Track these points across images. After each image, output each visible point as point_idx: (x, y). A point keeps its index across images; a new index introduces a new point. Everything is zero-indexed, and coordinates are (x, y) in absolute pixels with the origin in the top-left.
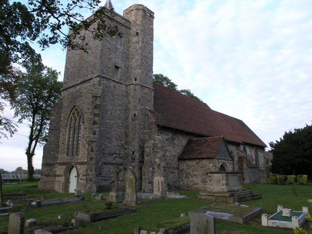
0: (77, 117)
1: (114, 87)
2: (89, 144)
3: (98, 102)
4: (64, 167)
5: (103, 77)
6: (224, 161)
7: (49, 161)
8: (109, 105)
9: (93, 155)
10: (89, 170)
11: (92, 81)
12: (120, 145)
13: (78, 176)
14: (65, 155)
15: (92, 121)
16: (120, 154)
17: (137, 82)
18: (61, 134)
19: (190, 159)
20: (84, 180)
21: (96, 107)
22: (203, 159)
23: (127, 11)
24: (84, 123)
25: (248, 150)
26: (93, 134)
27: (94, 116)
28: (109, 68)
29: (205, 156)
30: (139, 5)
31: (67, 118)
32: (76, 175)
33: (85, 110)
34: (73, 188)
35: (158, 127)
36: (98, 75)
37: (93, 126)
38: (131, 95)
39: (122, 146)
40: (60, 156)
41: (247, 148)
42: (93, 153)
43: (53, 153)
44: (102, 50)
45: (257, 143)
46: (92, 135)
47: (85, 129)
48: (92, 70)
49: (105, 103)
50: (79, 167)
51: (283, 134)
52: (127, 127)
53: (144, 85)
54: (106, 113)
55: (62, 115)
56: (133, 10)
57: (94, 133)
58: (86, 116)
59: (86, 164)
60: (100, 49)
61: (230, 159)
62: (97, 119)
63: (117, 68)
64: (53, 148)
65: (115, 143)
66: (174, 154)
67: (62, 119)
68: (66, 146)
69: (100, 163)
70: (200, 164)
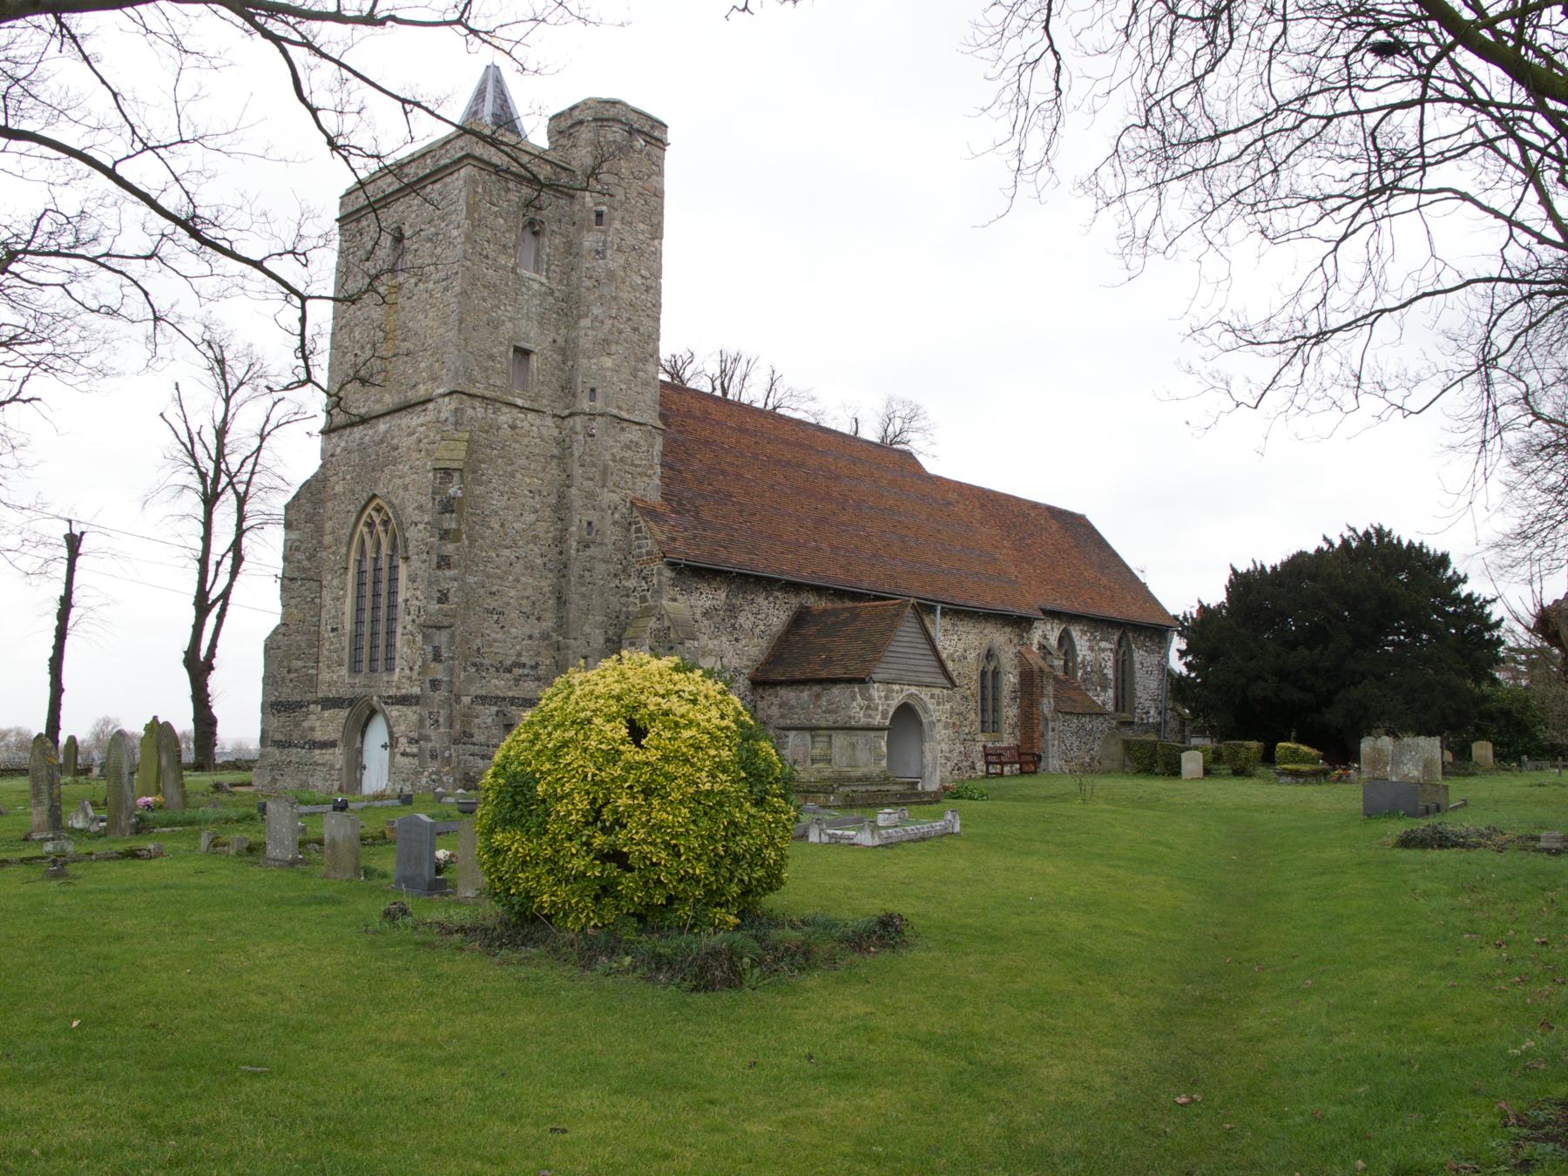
0: (382, 536)
1: (513, 427)
2: (425, 636)
3: (454, 490)
4: (345, 713)
5: (470, 395)
6: (913, 689)
7: (287, 693)
9: (439, 672)
10: (428, 722)
11: (431, 406)
12: (536, 633)
13: (392, 744)
14: (344, 671)
15: (435, 559)
16: (535, 667)
17: (599, 405)
18: (327, 596)
19: (792, 683)
20: (414, 756)
21: (448, 506)
22: (835, 681)
23: (564, 124)
24: (407, 559)
25: (1082, 642)
26: (440, 601)
27: (441, 538)
28: (491, 357)
29: (839, 672)
30: (607, 102)
31: (345, 539)
33: (410, 512)
34: (377, 775)
35: (673, 570)
36: (452, 387)
37: (439, 573)
38: (576, 454)
39: (545, 636)
40: (325, 676)
42: (440, 667)
43: (300, 663)
44: (464, 293)
45: (1136, 614)
46: (434, 607)
47: (412, 579)
49: (479, 490)
50: (394, 712)
51: (1224, 578)
52: (563, 570)
53: (625, 415)
55: (328, 525)
56: (581, 122)
57: (443, 598)
58: (412, 533)
59: (417, 703)
60: (457, 289)
62: (449, 548)
63: (523, 353)
64: (299, 647)
65: (519, 629)
66: (736, 662)
67: (328, 539)
69: (466, 700)
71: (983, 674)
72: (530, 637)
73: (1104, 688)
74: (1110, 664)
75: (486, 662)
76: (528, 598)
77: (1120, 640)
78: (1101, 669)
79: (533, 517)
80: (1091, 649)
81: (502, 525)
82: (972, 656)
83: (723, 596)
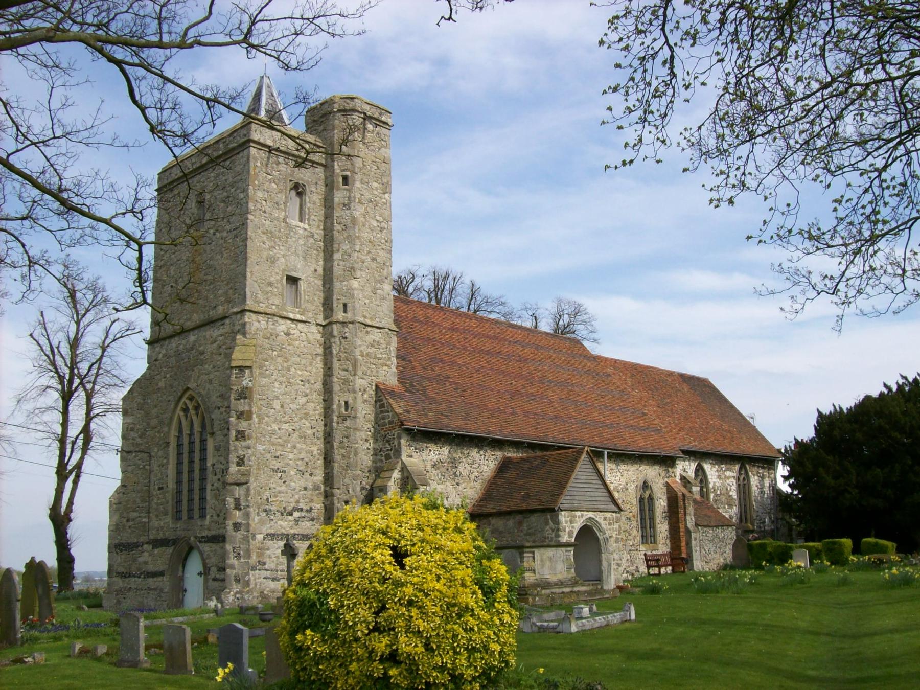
0: (194, 418)
1: (287, 334)
6: (591, 514)
8: (277, 384)
11: (227, 321)
12: (310, 486)
14: (168, 519)
16: (310, 510)
24: (212, 434)
28: (270, 284)
32: (200, 568)
41: (707, 467)
43: (135, 514)
48: (226, 293)
51: (813, 420)
53: (368, 322)
54: (269, 406)
61: (612, 507)
64: (135, 502)
65: (298, 483)
68: (169, 497)
70: (525, 527)
71: (641, 500)
72: (305, 489)
73: (730, 506)
74: (734, 487)
75: (274, 508)
76: (302, 459)
77: (740, 469)
78: (728, 491)
79: (304, 400)
80: (719, 477)
81: (282, 406)
82: (632, 487)
83: (446, 452)
